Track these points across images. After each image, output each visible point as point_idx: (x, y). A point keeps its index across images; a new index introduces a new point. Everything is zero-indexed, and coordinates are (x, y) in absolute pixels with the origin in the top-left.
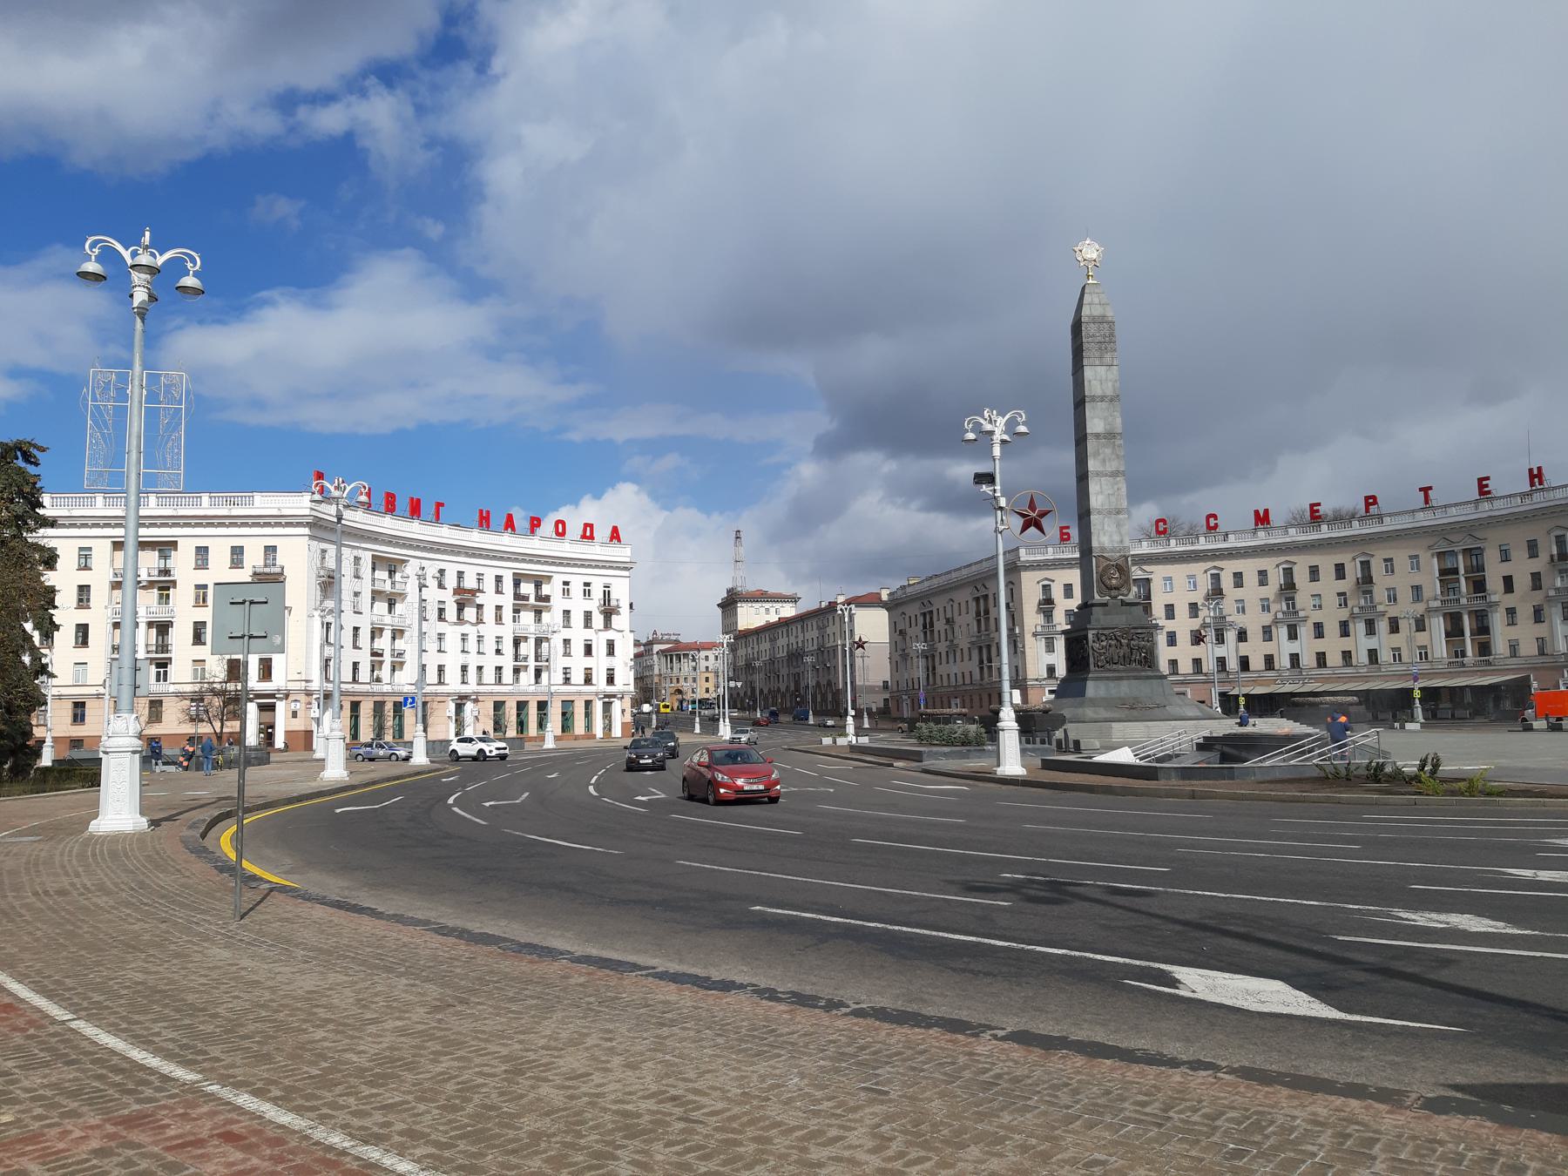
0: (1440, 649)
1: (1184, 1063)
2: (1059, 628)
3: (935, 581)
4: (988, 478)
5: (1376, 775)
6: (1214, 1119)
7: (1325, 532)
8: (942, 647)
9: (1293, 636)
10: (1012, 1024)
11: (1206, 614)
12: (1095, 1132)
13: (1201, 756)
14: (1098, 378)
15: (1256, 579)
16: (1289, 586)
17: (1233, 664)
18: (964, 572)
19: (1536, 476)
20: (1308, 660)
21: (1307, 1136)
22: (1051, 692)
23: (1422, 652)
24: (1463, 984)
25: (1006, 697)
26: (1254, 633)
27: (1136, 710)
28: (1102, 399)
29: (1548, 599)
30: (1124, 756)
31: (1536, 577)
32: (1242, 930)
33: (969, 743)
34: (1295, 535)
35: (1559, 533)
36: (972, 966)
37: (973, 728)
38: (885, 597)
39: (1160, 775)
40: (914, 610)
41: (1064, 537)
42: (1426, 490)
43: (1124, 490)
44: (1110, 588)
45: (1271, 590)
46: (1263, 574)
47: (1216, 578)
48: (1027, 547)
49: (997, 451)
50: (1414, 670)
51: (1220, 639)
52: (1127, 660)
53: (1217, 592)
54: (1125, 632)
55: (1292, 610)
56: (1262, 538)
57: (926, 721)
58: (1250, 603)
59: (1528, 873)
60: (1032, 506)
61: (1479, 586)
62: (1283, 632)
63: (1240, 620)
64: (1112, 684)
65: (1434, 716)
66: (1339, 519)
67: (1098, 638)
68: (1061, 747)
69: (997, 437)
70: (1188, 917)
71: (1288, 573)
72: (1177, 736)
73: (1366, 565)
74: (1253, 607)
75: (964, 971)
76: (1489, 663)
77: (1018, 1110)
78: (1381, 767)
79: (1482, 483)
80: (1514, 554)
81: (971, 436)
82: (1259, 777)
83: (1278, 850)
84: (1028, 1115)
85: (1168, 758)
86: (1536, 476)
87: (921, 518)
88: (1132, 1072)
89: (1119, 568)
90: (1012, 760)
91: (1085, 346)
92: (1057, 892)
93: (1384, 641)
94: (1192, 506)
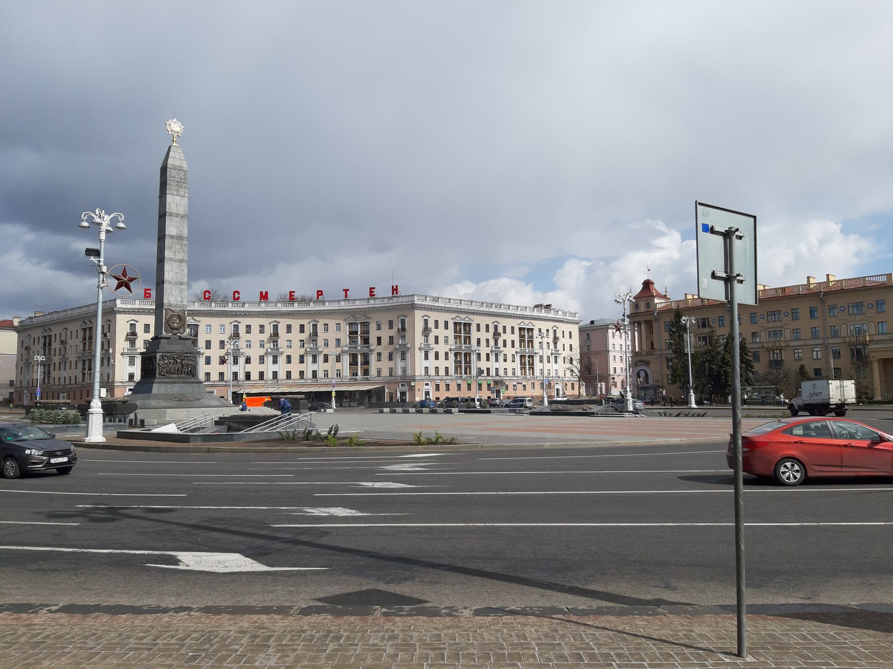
0: (346, 372)
1: (172, 609)
2: (139, 351)
3: (55, 316)
4: (97, 253)
5: (308, 436)
6: (183, 640)
7: (296, 307)
8: (56, 359)
9: (275, 361)
10: (64, 601)
11: (229, 347)
12: (108, 661)
13: (216, 428)
14: (176, 202)
15: (258, 329)
17: (241, 376)
18: (69, 313)
19: (395, 290)
20: (282, 375)
21: (236, 640)
22: (130, 390)
23: (335, 373)
24: (331, 544)
25: (96, 393)
26: (255, 360)
27: (182, 401)
28: (177, 215)
29: (395, 349)
30: (171, 429)
31: (391, 338)
32: (223, 527)
33: (69, 422)
34: (280, 307)
36: (45, 567)
37: (73, 413)
38: (16, 323)
39: (191, 439)
40: (37, 334)
41: (147, 295)
42: (346, 291)
43: (186, 272)
44: (173, 329)
45: (266, 336)
46: (262, 327)
47: (236, 327)
48: (121, 298)
49: (103, 236)
50: (334, 381)
51: (236, 362)
52: (179, 372)
53: (236, 335)
54: (180, 355)
56: (263, 307)
57: (38, 408)
58: (253, 343)
59: (370, 484)
60: (124, 274)
61: (366, 341)
62: (270, 359)
63: (247, 352)
64: (169, 386)
65: (341, 406)
66: (304, 301)
67: (162, 357)
68: (132, 424)
69: (104, 227)
70: (192, 522)
71: (276, 327)
72: (203, 417)
73: (315, 326)
74: (255, 344)
75: (38, 570)
76: (367, 379)
77: (56, 657)
78: (310, 432)
79: (371, 290)
80: (382, 327)
81: (86, 224)
82: (247, 439)
83: (250, 480)
84: (63, 659)
85: (198, 429)
86: (395, 290)
87: (51, 273)
88: (138, 620)
89: (179, 317)
90: (96, 431)
91: (168, 182)
92: (113, 514)
93: (321, 367)
94: (226, 286)
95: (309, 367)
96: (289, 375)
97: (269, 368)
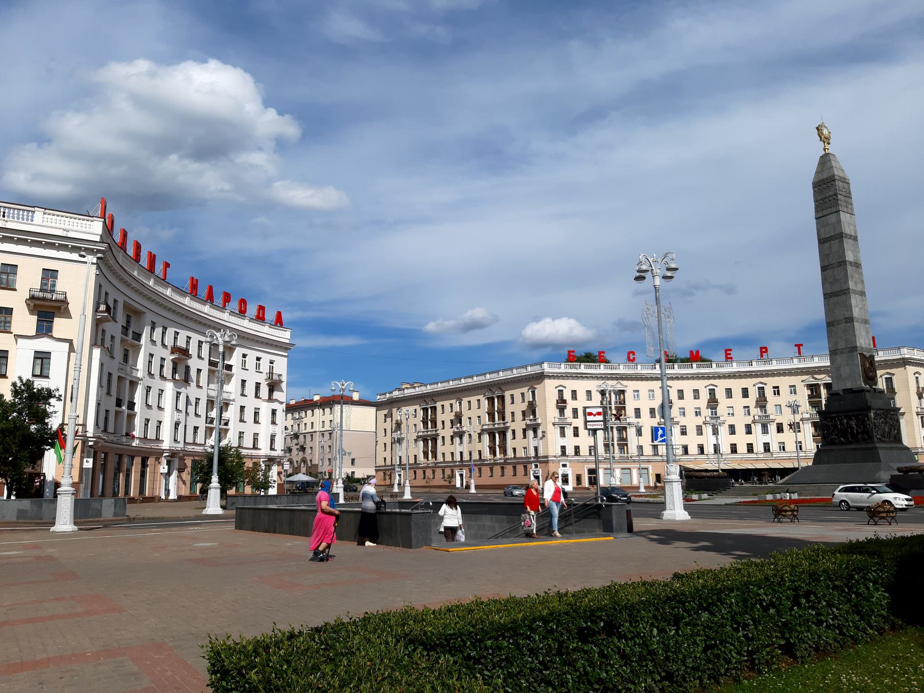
16: (713, 402)
26: (692, 430)
35: (561, 388)
45: (751, 401)
46: (696, 392)
55: (715, 416)
93: (773, 438)
95: (758, 438)
96: (767, 448)
97: (709, 440)
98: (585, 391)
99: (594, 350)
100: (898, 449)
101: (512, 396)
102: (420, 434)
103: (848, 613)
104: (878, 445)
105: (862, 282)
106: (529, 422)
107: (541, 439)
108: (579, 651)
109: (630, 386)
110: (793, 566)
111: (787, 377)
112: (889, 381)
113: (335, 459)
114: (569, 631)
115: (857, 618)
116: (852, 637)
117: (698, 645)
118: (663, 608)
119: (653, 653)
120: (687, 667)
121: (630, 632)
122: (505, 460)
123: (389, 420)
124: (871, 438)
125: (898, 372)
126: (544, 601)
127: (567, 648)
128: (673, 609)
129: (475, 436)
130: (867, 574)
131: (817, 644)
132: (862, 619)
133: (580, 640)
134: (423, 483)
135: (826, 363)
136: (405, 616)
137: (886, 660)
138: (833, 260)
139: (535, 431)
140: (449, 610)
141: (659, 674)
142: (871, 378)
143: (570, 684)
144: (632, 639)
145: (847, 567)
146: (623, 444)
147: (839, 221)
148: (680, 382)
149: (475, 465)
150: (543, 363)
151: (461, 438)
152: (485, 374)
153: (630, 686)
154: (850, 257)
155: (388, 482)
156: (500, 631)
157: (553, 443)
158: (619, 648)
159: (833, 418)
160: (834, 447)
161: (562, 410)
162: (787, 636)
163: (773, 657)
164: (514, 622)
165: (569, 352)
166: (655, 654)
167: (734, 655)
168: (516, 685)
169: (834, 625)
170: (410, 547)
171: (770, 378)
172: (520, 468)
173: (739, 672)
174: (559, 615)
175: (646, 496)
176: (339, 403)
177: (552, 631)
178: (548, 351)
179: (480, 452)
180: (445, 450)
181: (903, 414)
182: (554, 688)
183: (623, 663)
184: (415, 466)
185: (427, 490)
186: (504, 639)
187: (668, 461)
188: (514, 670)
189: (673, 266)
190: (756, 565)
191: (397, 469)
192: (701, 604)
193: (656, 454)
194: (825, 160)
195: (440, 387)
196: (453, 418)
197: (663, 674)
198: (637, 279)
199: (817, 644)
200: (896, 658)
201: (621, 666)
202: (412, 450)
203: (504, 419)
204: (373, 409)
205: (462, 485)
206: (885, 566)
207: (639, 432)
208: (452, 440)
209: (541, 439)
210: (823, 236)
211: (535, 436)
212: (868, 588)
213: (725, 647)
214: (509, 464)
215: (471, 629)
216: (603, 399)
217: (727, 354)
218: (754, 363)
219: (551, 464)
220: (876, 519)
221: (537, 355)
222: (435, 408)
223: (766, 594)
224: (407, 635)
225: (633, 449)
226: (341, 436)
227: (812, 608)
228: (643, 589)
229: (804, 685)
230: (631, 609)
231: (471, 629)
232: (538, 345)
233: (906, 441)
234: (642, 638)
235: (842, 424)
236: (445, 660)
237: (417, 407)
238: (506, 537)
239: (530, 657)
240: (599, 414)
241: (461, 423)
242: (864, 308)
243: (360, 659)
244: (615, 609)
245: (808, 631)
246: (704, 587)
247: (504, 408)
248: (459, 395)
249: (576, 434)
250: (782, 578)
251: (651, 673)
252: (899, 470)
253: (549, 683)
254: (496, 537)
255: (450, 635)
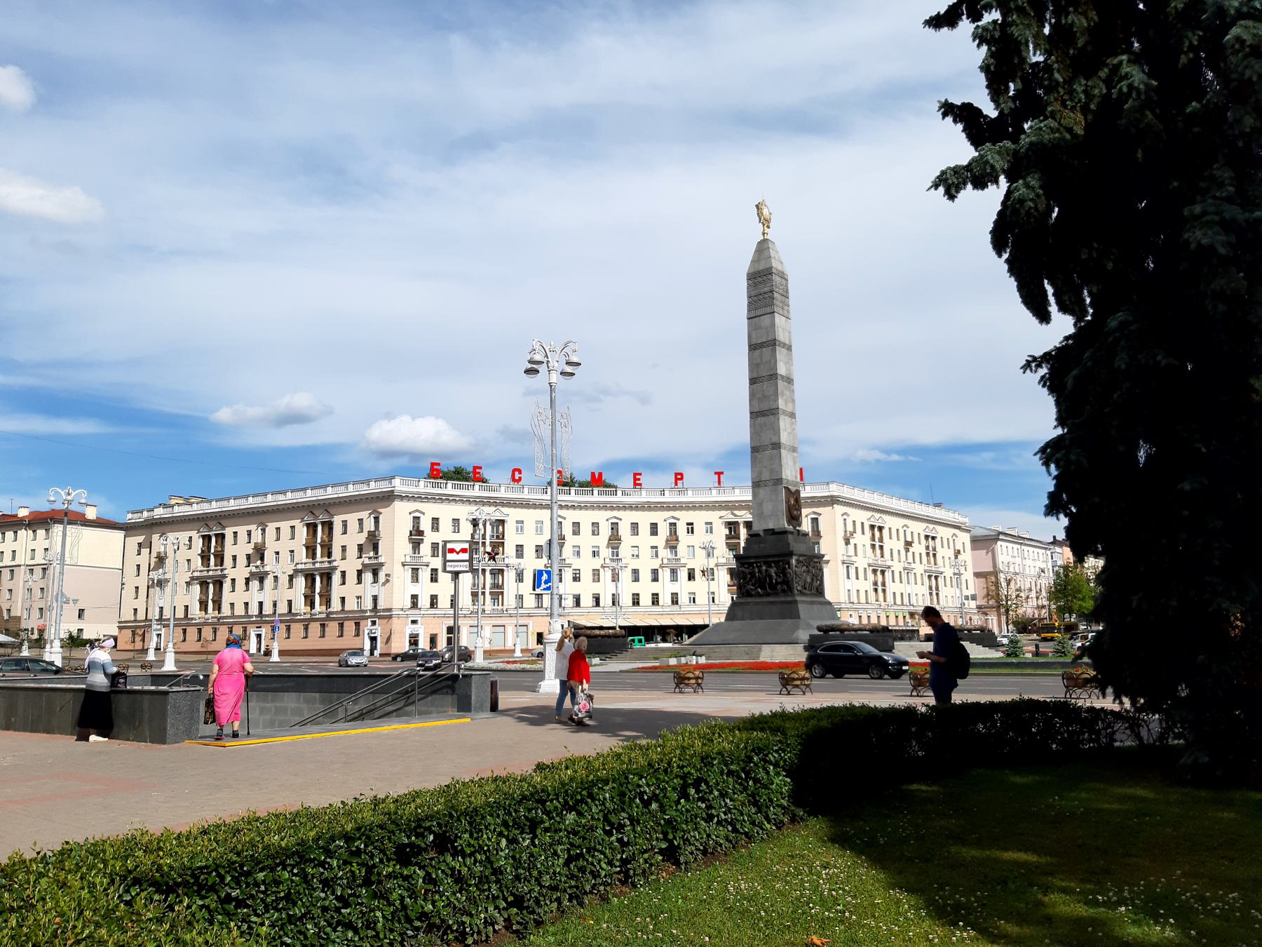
15: (590, 528)
16: (615, 540)
26: (586, 576)
35: (417, 514)
46: (595, 525)
71: (614, 527)
93: (683, 587)
97: (606, 589)
98: (452, 518)
99: (467, 464)
100: (820, 603)
101: (345, 523)
102: (196, 574)
103: (743, 804)
104: (798, 598)
105: (793, 401)
106: (367, 561)
107: (384, 584)
108: (396, 878)
109: (512, 515)
110: (683, 748)
111: (704, 512)
112: (815, 521)
113: (50, 609)
114: (383, 851)
115: (753, 810)
116: (746, 834)
117: (559, 857)
118: (516, 811)
119: (497, 872)
120: (542, 886)
121: (469, 845)
122: (328, 614)
123: (145, 551)
124: (790, 589)
125: (824, 511)
126: (348, 812)
127: (379, 874)
128: (530, 810)
129: (284, 580)
130: (767, 755)
131: (706, 845)
132: (759, 811)
133: (399, 861)
134: (197, 647)
135: (748, 496)
136: (129, 846)
137: (781, 860)
138: (764, 372)
139: (375, 574)
140: (205, 832)
141: (505, 899)
142: (794, 518)
143: (380, 925)
144: (472, 854)
145: (746, 748)
146: (498, 592)
147: (773, 324)
148: (577, 512)
149: (281, 621)
150: (393, 477)
151: (261, 580)
152: (305, 489)
153: (465, 919)
154: (782, 370)
155: (139, 645)
156: (280, 858)
157: (398, 590)
158: (453, 869)
159: (750, 565)
160: (750, 600)
161: (416, 545)
162: (670, 836)
163: (651, 865)
164: (302, 843)
165: (433, 464)
166: (501, 873)
167: (604, 866)
168: (300, 932)
169: (726, 820)
170: (162, 741)
171: (684, 512)
172: (350, 627)
173: (608, 888)
174: (371, 830)
175: (521, 662)
176: (61, 522)
177: (358, 853)
178: (403, 462)
179: (290, 602)
180: (235, 599)
181: (828, 562)
182: (356, 931)
183: (457, 888)
184: (185, 623)
185: (203, 657)
186: (284, 869)
187: (551, 615)
188: (298, 911)
189: (574, 359)
190: (641, 748)
191: (155, 627)
192: (566, 802)
193: (539, 606)
194: (763, 247)
195: (232, 505)
196: (251, 552)
197: (511, 899)
198: (528, 371)
199: (706, 845)
200: (792, 856)
201: (454, 894)
202: (181, 598)
203: (329, 555)
204: (119, 535)
205: (259, 649)
206: (788, 745)
207: (520, 577)
208: (247, 583)
209: (384, 584)
210: (754, 341)
211: (375, 581)
212: (768, 773)
213: (593, 856)
214: (334, 619)
215: (235, 858)
216: (475, 531)
217: (635, 479)
218: (667, 493)
219: (394, 620)
220: (789, 688)
221: (384, 466)
222: (223, 536)
223: (648, 785)
224: (130, 872)
225: (509, 600)
226: (62, 573)
227: (702, 800)
228: (493, 786)
229: (685, 898)
230: (474, 817)
231: (235, 858)
232: (387, 454)
233: (829, 595)
234: (485, 852)
235: (760, 572)
236: (185, 905)
237: (194, 534)
238: (318, 724)
239: (323, 891)
240: (464, 551)
241: (262, 559)
242: (792, 433)
243: (44, 917)
244: (451, 816)
245: (696, 829)
246: (572, 779)
247: (331, 539)
248: (262, 518)
249: (434, 579)
250: (669, 764)
251: (495, 898)
252: (819, 629)
253: (349, 926)
254: (303, 723)
255: (201, 868)
